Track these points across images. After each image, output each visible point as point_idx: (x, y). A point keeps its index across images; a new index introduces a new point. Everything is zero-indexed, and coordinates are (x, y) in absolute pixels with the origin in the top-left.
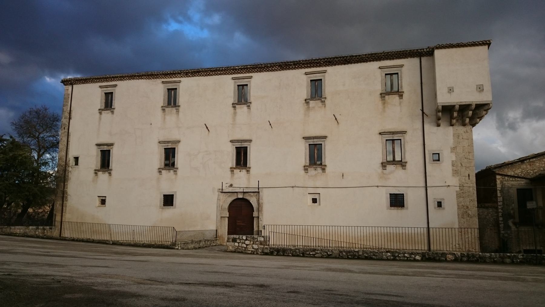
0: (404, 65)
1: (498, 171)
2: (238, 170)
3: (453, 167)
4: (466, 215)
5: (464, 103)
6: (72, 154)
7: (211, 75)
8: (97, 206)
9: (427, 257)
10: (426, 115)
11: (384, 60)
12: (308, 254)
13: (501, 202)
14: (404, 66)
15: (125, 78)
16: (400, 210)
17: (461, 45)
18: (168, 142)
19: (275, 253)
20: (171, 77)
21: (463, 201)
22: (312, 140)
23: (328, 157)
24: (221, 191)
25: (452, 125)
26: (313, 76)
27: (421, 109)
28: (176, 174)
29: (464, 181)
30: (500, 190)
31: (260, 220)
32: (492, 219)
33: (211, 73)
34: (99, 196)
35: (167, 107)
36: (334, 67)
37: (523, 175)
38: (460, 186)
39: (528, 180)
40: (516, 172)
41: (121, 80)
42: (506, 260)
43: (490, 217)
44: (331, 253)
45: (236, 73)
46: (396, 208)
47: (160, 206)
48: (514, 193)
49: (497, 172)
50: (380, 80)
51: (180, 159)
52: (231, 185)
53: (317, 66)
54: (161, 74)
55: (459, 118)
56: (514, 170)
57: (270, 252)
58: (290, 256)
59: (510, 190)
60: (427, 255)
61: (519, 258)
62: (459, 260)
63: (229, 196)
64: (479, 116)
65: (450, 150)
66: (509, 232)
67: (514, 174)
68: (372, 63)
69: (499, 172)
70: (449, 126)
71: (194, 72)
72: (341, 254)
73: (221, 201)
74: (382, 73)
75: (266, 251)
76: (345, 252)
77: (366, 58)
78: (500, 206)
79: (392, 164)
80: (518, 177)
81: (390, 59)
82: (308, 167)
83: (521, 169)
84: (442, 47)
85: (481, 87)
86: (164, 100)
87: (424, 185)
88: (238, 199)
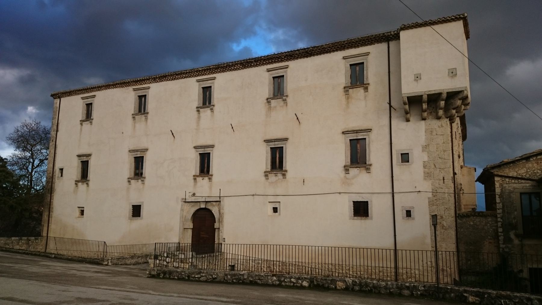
0: (369, 53)
1: (497, 171)
2: (201, 178)
3: (425, 168)
4: (440, 227)
5: (434, 92)
6: (58, 166)
7: (177, 79)
8: (77, 216)
9: (315, 283)
10: (394, 108)
11: (348, 49)
12: (193, 277)
13: (500, 209)
14: (370, 54)
15: (102, 88)
16: (363, 220)
17: (430, 23)
18: (137, 151)
19: (161, 275)
20: (141, 84)
22: (273, 143)
23: (289, 163)
24: (184, 201)
25: (424, 119)
26: (275, 72)
27: (389, 103)
28: (144, 183)
29: (437, 185)
30: (499, 195)
31: (220, 231)
32: (492, 230)
33: (177, 77)
34: (79, 207)
35: (136, 114)
36: (296, 61)
37: (528, 176)
38: (433, 191)
39: (534, 182)
40: (519, 172)
41: (99, 90)
42: (404, 292)
43: (489, 227)
44: (216, 276)
45: (201, 75)
46: (359, 218)
47: (129, 217)
48: (516, 197)
49: (496, 173)
50: (344, 72)
51: (148, 168)
52: (194, 194)
53: (278, 62)
54: (131, 81)
55: (432, 110)
56: (517, 170)
57: (157, 275)
58: (175, 279)
59: (512, 195)
60: (316, 280)
61: (419, 290)
62: (350, 289)
63: (193, 206)
64: (454, 107)
65: (421, 149)
67: (517, 175)
68: (336, 53)
69: (498, 173)
70: (421, 120)
71: (161, 76)
72: (226, 277)
73: (185, 211)
74: (346, 63)
75: (153, 273)
76: (230, 275)
77: (329, 49)
78: (499, 214)
79: (356, 167)
80: (522, 179)
81: (355, 47)
82: (268, 173)
85: (454, 71)
86: (135, 108)
87: (390, 190)
88: (201, 209)
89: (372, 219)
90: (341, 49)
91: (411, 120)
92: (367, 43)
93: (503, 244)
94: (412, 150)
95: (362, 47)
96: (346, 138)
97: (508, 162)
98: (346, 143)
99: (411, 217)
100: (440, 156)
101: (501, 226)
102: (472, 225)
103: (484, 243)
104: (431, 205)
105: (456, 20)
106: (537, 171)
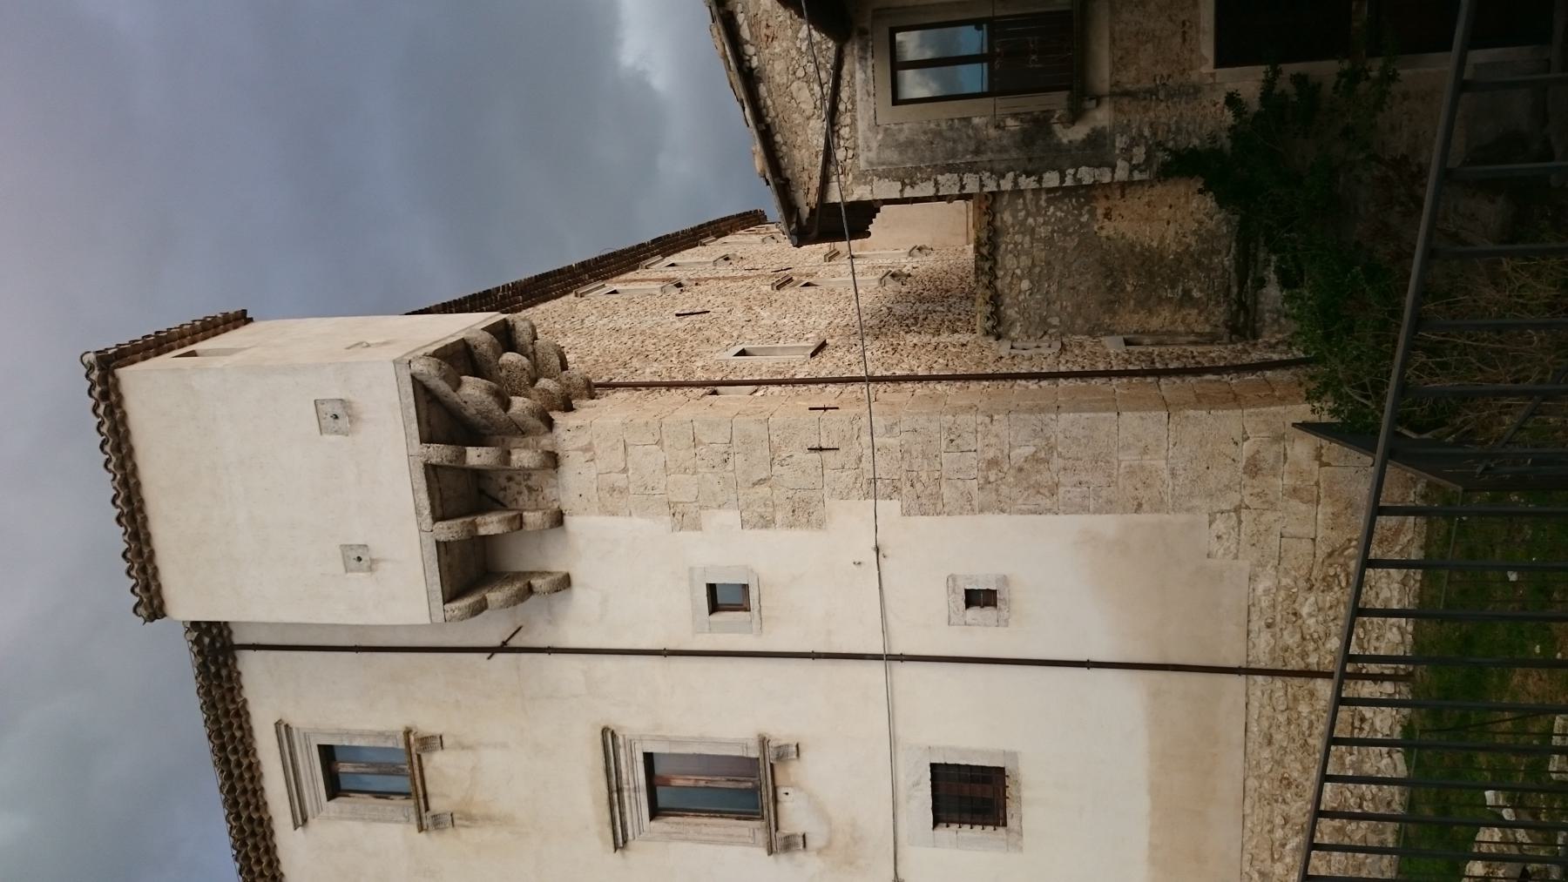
13: (961, 180)
16: (1019, 791)
21: (960, 483)
25: (559, 519)
27: (488, 655)
29: (847, 477)
30: (904, 185)
32: (1052, 209)
39: (847, 50)
40: (808, 107)
43: (1041, 220)
49: (813, 198)
50: (358, 828)
55: (519, 484)
59: (902, 138)
65: (687, 536)
66: (1120, 142)
69: (813, 191)
70: (565, 531)
74: (323, 814)
78: (982, 186)
79: (776, 801)
83: (795, 84)
84: (147, 588)
85: (329, 409)
87: (878, 666)
89: (1014, 756)
90: (265, 833)
91: (564, 570)
92: (238, 734)
93: (1113, 168)
94: (691, 569)
95: (255, 750)
96: (643, 835)
97: (762, 154)
98: (669, 837)
99: (995, 592)
100: (718, 460)
101: (1033, 178)
102: (1031, 282)
103: (1108, 238)
104: (940, 506)
105: (113, 398)
106: (802, 40)
